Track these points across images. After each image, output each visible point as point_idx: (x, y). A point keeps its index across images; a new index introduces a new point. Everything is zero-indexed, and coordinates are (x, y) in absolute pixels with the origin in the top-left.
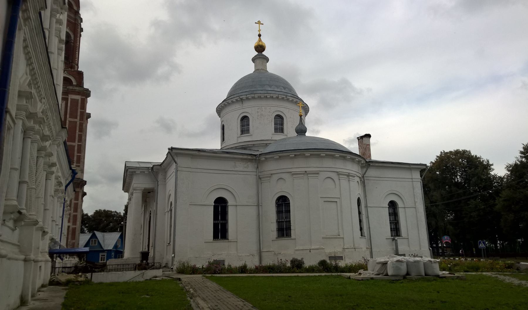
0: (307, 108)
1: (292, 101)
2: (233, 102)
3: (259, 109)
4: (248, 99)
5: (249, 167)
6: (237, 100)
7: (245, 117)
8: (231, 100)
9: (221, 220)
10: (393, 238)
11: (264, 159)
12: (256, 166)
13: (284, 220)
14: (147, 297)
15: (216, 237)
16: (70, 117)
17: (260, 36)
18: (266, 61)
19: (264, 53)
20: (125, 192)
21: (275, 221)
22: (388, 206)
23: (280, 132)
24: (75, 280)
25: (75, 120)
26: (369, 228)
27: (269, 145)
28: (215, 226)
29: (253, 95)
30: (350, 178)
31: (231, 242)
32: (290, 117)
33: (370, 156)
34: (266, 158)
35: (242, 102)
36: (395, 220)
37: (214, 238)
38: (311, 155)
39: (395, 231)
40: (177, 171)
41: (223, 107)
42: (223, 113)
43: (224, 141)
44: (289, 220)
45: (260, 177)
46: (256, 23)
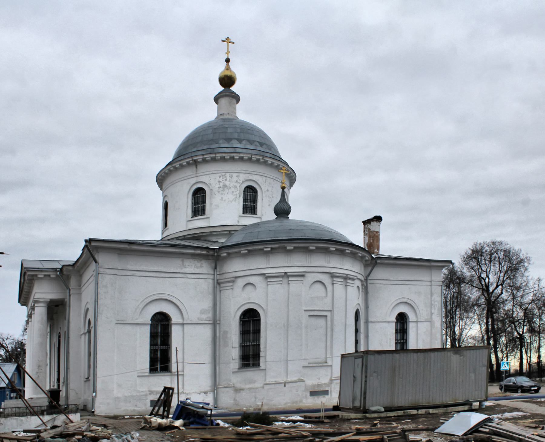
1: (273, 163)
8: (180, 163)
13: (250, 344)
17: (228, 61)
18: (235, 101)
19: (233, 88)
20: (22, 305)
28: (153, 353)
30: (349, 281)
42: (167, 182)
46: (223, 41)
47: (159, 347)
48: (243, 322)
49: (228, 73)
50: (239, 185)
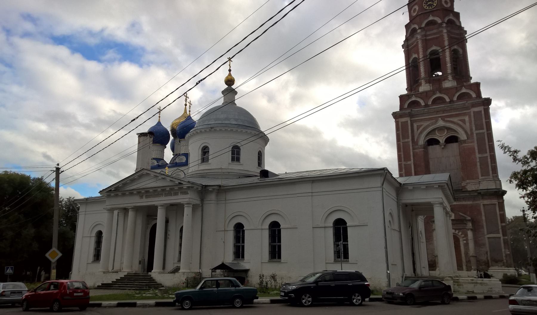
8: (220, 128)
16: (476, 130)
17: (230, 70)
25: (478, 132)
33: (521, 216)
41: (190, 136)
47: (241, 245)
49: (230, 77)
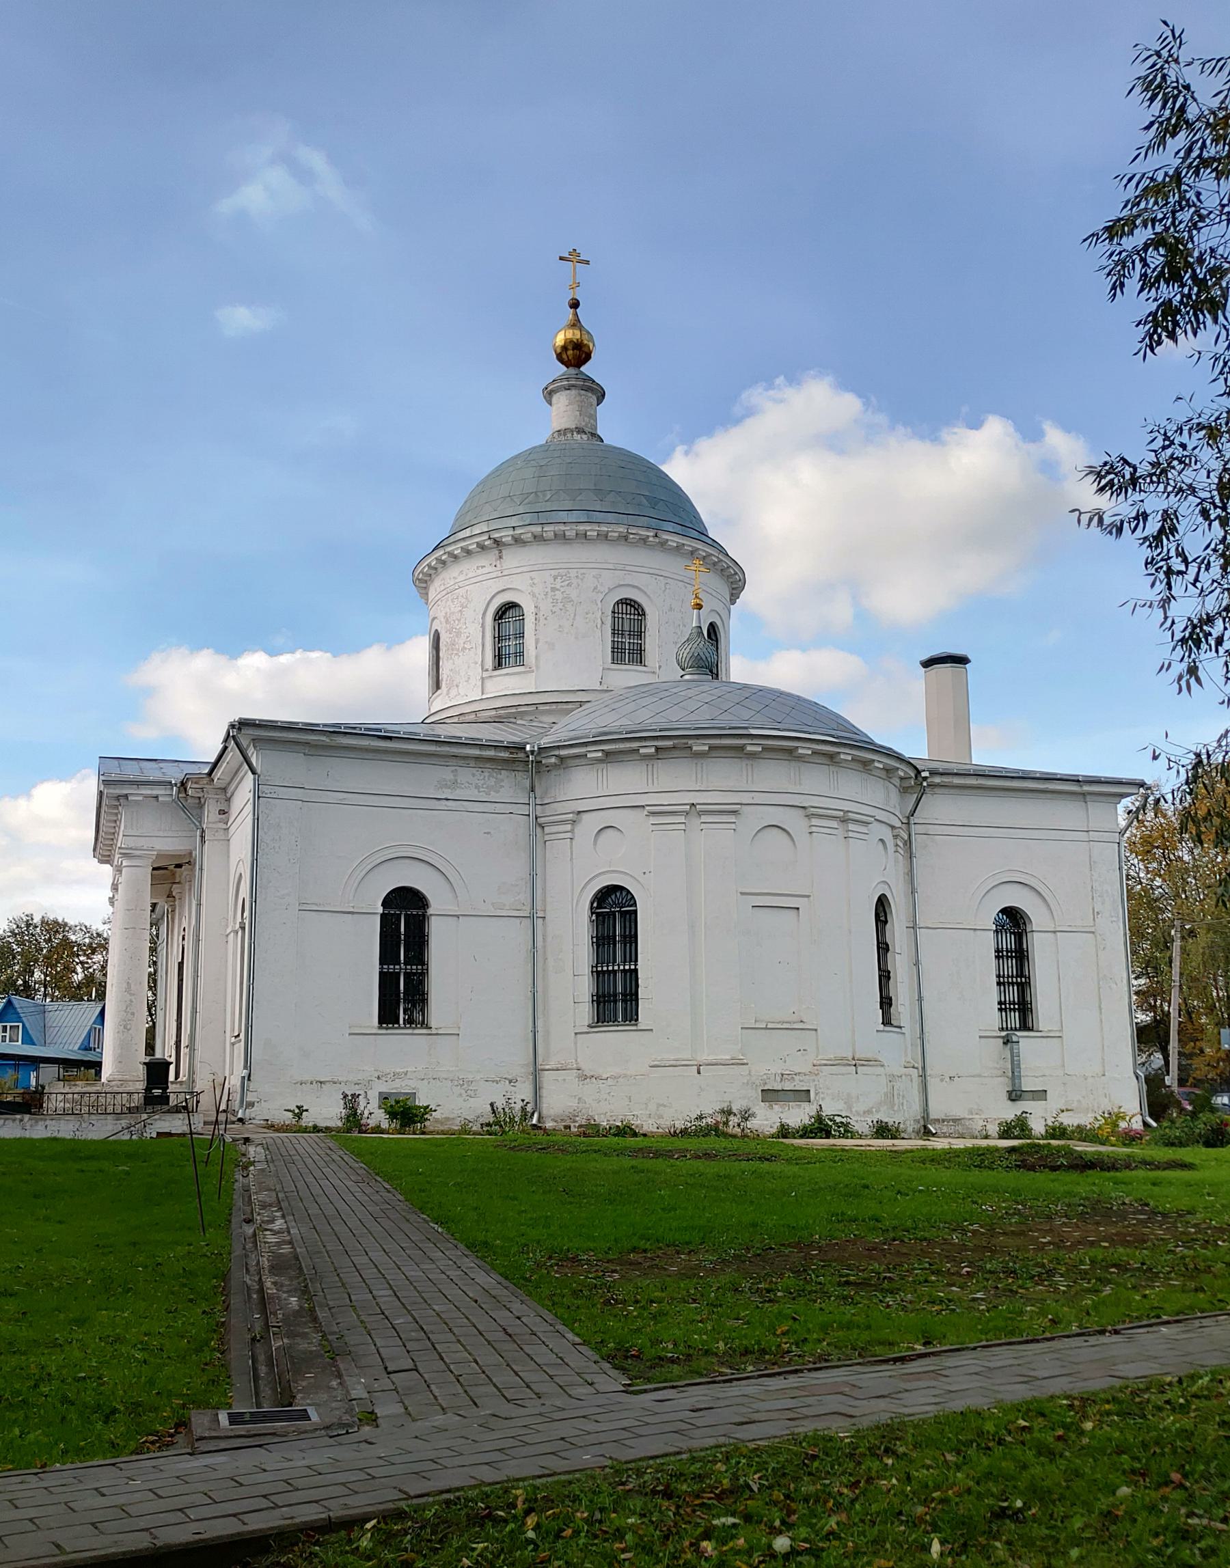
0: (736, 573)
1: (679, 547)
2: (468, 552)
3: (559, 580)
4: (517, 541)
5: (502, 786)
6: (482, 547)
7: (510, 608)
8: (463, 544)
9: (405, 964)
10: (1004, 1034)
11: (553, 760)
12: (527, 783)
13: (616, 968)
14: (1142, 1217)
15: (387, 1016)
17: (575, 305)
20: (101, 862)
21: (586, 970)
22: (994, 927)
23: (631, 661)
24: (442, 1124)
26: (920, 999)
27: (1183, 549)
28: (387, 982)
29: (537, 529)
30: (851, 827)
31: (437, 1034)
32: (671, 609)
34: (562, 759)
35: (500, 551)
36: (1021, 974)
37: (380, 1022)
38: (711, 748)
39: (1017, 1014)
40: (258, 797)
43: (439, 691)
44: (633, 967)
45: (541, 820)
46: (561, 258)
48: (597, 917)
50: (601, 596)
